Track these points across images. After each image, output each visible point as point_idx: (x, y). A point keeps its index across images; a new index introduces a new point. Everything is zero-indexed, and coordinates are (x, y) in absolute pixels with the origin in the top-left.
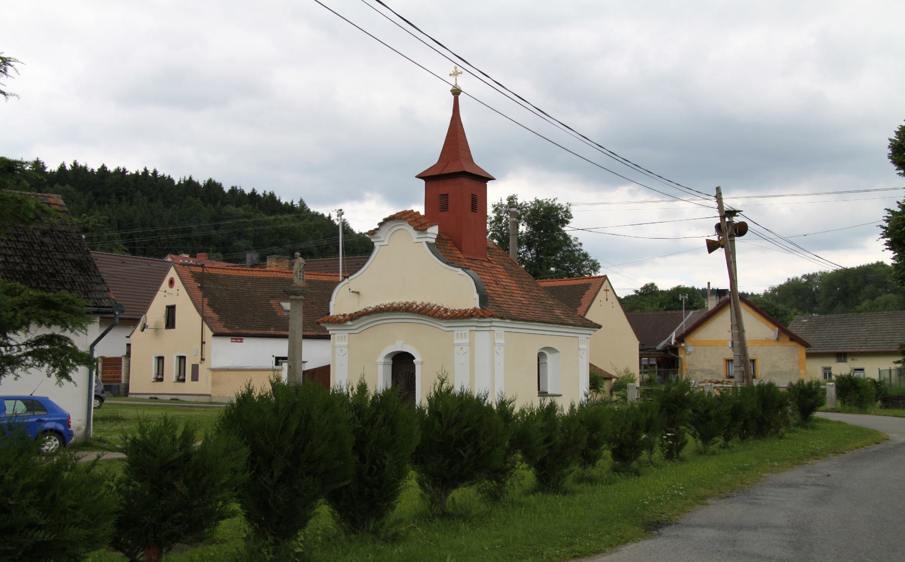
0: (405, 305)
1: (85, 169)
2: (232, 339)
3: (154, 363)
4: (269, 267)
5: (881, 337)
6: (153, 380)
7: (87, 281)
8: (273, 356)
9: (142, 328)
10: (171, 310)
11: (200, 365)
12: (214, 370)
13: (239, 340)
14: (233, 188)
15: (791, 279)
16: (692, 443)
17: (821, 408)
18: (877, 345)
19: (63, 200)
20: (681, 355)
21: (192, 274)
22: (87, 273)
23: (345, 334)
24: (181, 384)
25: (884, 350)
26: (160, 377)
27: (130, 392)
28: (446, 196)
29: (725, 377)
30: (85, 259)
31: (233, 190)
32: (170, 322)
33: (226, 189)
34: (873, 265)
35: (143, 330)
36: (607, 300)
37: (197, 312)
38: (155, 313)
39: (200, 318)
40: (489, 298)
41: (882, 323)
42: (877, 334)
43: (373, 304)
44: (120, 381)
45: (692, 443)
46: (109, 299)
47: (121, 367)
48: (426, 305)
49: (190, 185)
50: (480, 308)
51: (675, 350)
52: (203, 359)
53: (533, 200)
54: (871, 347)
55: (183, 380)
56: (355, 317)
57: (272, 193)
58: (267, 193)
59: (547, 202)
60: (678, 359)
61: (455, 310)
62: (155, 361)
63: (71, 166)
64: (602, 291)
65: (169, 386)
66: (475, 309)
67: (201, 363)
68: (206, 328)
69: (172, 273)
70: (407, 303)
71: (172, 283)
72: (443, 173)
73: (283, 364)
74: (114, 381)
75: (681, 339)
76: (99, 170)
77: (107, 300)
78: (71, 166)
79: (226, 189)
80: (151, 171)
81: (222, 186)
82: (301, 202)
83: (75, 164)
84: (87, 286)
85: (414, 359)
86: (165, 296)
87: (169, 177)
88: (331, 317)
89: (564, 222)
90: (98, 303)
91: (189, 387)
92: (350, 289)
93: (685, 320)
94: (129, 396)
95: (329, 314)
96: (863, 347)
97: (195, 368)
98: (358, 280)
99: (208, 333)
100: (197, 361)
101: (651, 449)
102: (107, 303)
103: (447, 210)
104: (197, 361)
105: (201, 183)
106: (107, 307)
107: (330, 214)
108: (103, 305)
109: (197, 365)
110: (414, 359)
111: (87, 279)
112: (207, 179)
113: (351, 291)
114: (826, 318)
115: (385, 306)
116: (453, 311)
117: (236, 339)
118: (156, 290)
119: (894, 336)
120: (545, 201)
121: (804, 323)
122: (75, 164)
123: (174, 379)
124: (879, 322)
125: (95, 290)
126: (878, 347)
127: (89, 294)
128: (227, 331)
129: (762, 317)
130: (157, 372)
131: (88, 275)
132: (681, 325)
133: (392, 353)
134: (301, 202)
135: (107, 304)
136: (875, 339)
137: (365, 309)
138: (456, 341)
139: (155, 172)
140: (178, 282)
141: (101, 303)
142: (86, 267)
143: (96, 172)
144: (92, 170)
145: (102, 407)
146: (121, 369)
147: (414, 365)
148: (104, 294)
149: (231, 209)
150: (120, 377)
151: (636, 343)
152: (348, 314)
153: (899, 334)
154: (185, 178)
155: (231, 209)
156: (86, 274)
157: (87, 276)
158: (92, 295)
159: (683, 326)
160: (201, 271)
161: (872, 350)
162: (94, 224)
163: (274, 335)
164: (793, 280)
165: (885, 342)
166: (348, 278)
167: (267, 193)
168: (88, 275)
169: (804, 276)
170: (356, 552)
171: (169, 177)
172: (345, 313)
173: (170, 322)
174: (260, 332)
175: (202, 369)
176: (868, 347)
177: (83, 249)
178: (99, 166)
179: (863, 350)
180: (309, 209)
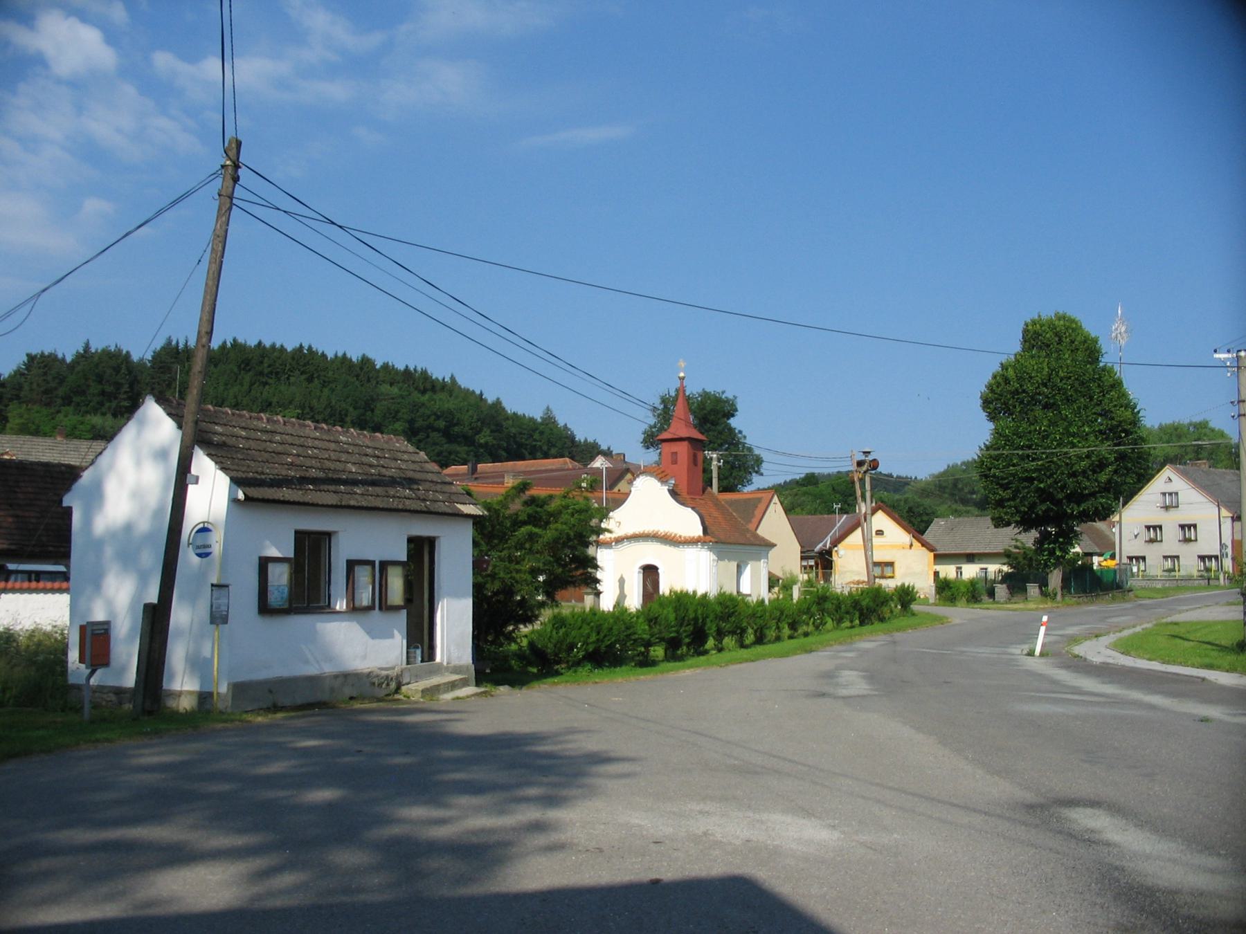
4: (507, 483)
15: (951, 465)
16: (830, 624)
17: (915, 602)
19: (434, 461)
20: (835, 557)
28: (676, 453)
31: (386, 367)
36: (775, 511)
43: (630, 532)
45: (830, 624)
51: (829, 553)
53: (700, 391)
57: (424, 369)
58: (419, 369)
59: (714, 394)
60: (831, 562)
64: (772, 504)
66: (700, 537)
75: (836, 543)
78: (225, 342)
80: (306, 346)
89: (731, 414)
93: (838, 525)
101: (808, 624)
105: (354, 359)
116: (685, 538)
120: (713, 393)
121: (941, 526)
132: (833, 531)
134: (452, 378)
139: (310, 348)
149: (385, 388)
151: (798, 548)
155: (385, 388)
159: (835, 531)
164: (953, 466)
167: (419, 369)
169: (963, 463)
170: (1008, 468)
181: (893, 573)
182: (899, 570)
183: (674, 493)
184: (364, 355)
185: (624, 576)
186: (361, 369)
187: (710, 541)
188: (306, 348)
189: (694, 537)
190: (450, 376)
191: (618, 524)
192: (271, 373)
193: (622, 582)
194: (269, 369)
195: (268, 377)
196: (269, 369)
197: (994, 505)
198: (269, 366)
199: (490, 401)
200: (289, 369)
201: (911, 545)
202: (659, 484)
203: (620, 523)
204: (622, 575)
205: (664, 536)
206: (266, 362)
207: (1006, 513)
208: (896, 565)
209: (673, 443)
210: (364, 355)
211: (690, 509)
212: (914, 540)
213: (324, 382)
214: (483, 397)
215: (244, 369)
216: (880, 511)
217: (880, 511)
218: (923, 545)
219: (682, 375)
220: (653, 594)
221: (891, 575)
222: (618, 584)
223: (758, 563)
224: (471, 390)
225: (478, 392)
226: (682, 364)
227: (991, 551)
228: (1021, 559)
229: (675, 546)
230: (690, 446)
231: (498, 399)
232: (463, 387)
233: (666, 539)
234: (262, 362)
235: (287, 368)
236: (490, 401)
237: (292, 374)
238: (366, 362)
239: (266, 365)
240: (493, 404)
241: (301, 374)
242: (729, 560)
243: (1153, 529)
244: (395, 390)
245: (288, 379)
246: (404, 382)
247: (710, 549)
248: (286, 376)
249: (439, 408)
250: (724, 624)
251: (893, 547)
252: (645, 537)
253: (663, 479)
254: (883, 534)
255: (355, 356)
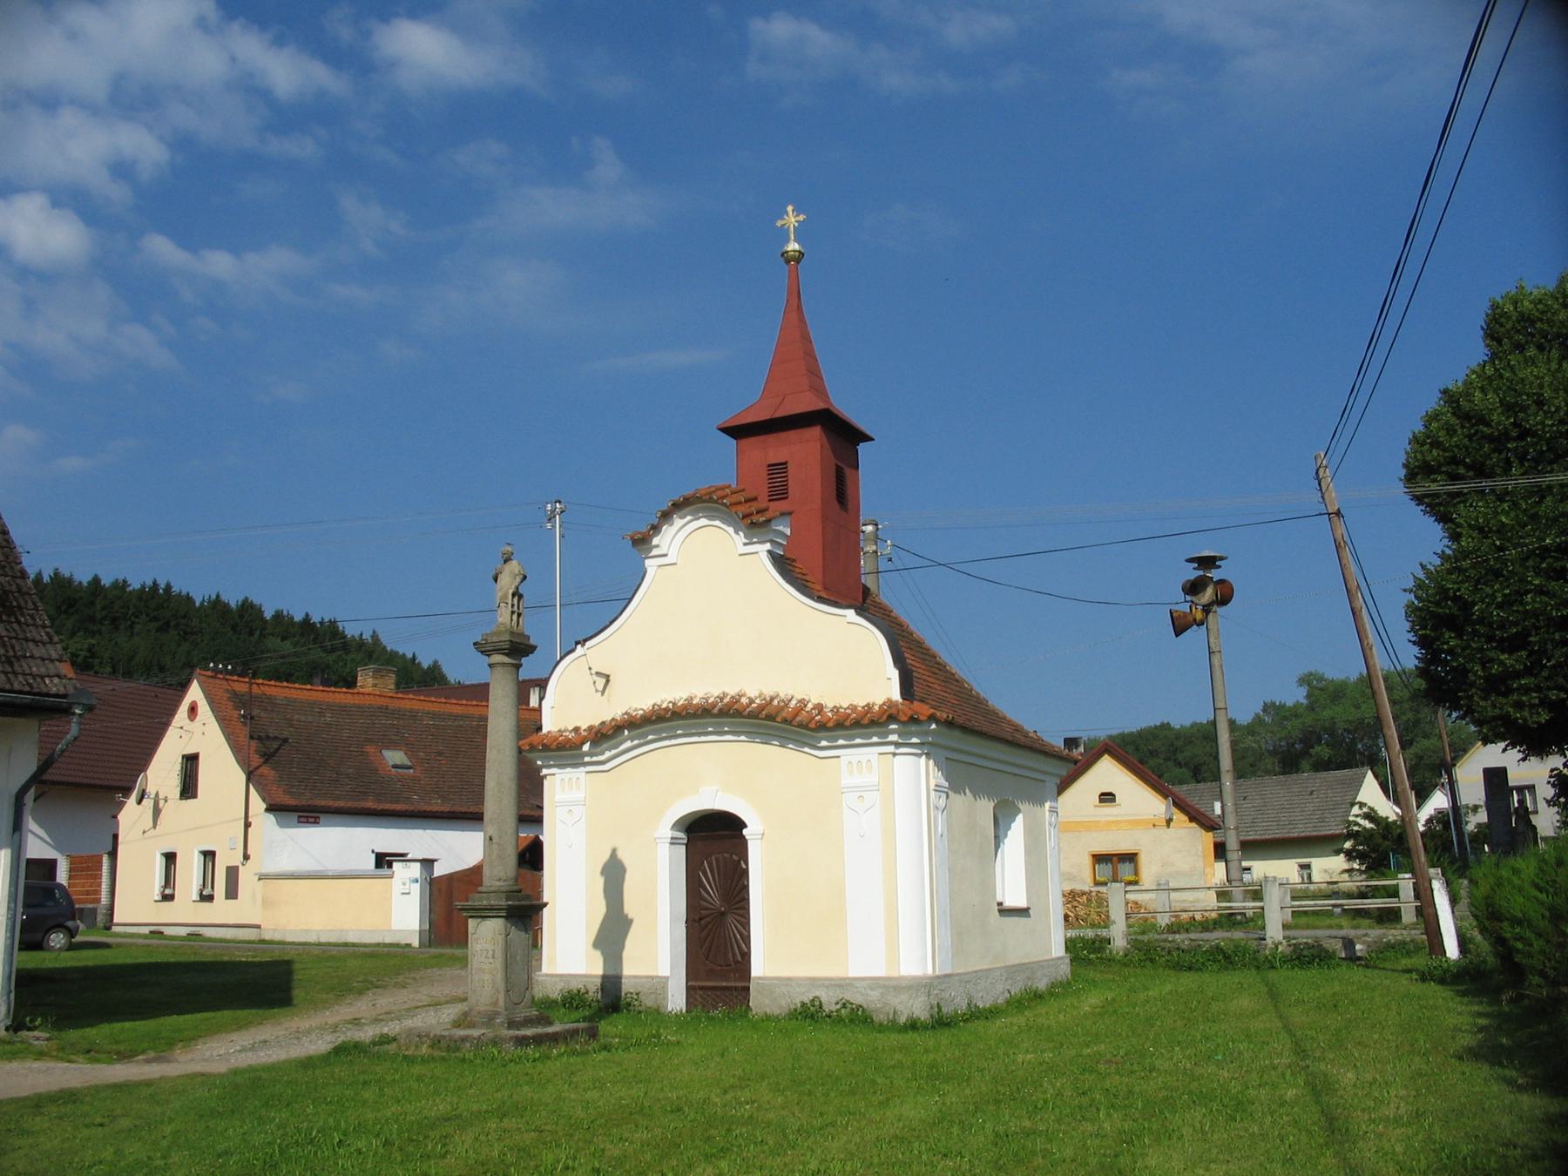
0: (721, 699)
1: (70, 580)
2: (299, 817)
3: (159, 863)
5: (1273, 816)
6: (157, 898)
7: (13, 634)
8: (1468, 367)
9: (139, 797)
10: (191, 761)
11: (241, 868)
12: (262, 877)
13: (313, 820)
14: (277, 612)
18: (1270, 828)
21: (228, 695)
22: (16, 618)
23: (578, 775)
24: (206, 905)
25: (1280, 836)
26: (168, 891)
27: (115, 921)
29: (1092, 885)
30: (14, 588)
32: (189, 788)
33: (268, 614)
34: (1156, 727)
35: (139, 802)
37: (237, 766)
38: (162, 773)
39: (243, 777)
40: (915, 674)
41: (1272, 794)
42: (1267, 812)
43: (641, 701)
44: (98, 901)
46: (59, 676)
47: (101, 874)
48: (772, 699)
49: (217, 606)
50: (901, 700)
52: (246, 857)
54: (1262, 832)
55: (210, 898)
56: (605, 735)
61: (841, 707)
62: (161, 862)
63: (50, 576)
65: (185, 913)
66: (890, 703)
67: (243, 865)
68: (254, 795)
69: (195, 693)
70: (725, 695)
71: (193, 710)
72: (777, 415)
73: (394, 864)
74: (87, 901)
76: (89, 583)
77: (56, 680)
78: (50, 576)
79: (268, 614)
81: (263, 609)
82: (375, 635)
83: (56, 574)
84: (13, 647)
85: (745, 826)
86: (181, 737)
87: (188, 594)
88: (546, 735)
90: (35, 685)
91: (222, 911)
92: (590, 669)
94: (115, 929)
95: (540, 728)
96: (1251, 833)
97: (232, 873)
98: (600, 651)
99: (258, 805)
100: (237, 859)
102: (56, 686)
103: (786, 498)
104: (237, 859)
105: (233, 605)
106: (56, 696)
107: (414, 654)
108: (45, 690)
109: (236, 868)
110: (745, 826)
111: (14, 630)
112: (241, 599)
113: (593, 672)
114: (1190, 790)
115: (674, 704)
116: (835, 710)
117: (307, 817)
118: (165, 726)
119: (1292, 814)
122: (56, 574)
123: (195, 896)
124: (1268, 792)
125: (32, 657)
126: (1272, 832)
127: (16, 665)
128: (292, 802)
129: (1140, 782)
130: (163, 883)
131: (19, 622)
133: (677, 821)
134: (375, 635)
135: (54, 690)
136: (1266, 820)
137: (626, 713)
138: (846, 781)
139: (168, 587)
140: (204, 708)
141: (42, 686)
142: (15, 604)
143: (86, 587)
144: (80, 583)
145: (1272, 975)
146: (101, 878)
147: (746, 841)
148: (51, 666)
150: (98, 892)
152: (584, 727)
153: (1299, 809)
154: (210, 597)
155: (272, 642)
156: (13, 620)
157: (15, 626)
158: (21, 666)
160: (247, 690)
161: (1263, 837)
162: (74, 651)
163: (374, 809)
165: (1281, 823)
166: (583, 645)
168: (19, 622)
171: (188, 594)
172: (578, 725)
173: (189, 788)
174: (350, 804)
175: (246, 877)
176: (1258, 833)
177: (12, 568)
178: (90, 578)
179: (1251, 838)
180: (385, 647)
181: (1136, 873)
182: (1149, 871)
183: (784, 564)
184: (247, 598)
185: (621, 855)
186: (241, 616)
187: (932, 718)
188: (163, 586)
189: (869, 707)
190: (371, 633)
191: (601, 682)
192: (105, 618)
193: (614, 873)
194: (104, 613)
195: (101, 623)
196: (104, 613)
197: (1482, 690)
198: (103, 609)
199: (425, 665)
200: (133, 614)
201: (1169, 822)
202: (740, 538)
203: (607, 678)
204: (614, 852)
205: (762, 708)
206: (99, 603)
207: (1519, 706)
208: (1143, 860)
209: (771, 438)
210: (247, 598)
211: (850, 614)
212: (1175, 810)
213: (186, 633)
214: (417, 662)
215: (66, 612)
216: (1106, 756)
217: (1106, 756)
218: (1192, 819)
219: (793, 246)
220: (723, 914)
221: (1132, 878)
222: (600, 882)
223: (1037, 809)
224: (401, 653)
225: (409, 655)
226: (792, 219)
227: (1258, 837)
228: (1379, 840)
229: (801, 743)
230: (827, 445)
231: (436, 662)
232: (389, 649)
233: (770, 717)
234: (92, 603)
235: (130, 612)
236: (425, 665)
237: (137, 620)
238: (248, 608)
239: (99, 607)
240: (429, 668)
241: (150, 621)
242: (976, 794)
243: (1517, 793)
244: (287, 646)
245: (131, 627)
246: (302, 635)
247: (929, 749)
248: (129, 623)
249: (351, 672)
250: (1294, 1092)
251: (1136, 823)
252: (695, 716)
253: (753, 523)
254: (1113, 800)
255: (233, 599)
